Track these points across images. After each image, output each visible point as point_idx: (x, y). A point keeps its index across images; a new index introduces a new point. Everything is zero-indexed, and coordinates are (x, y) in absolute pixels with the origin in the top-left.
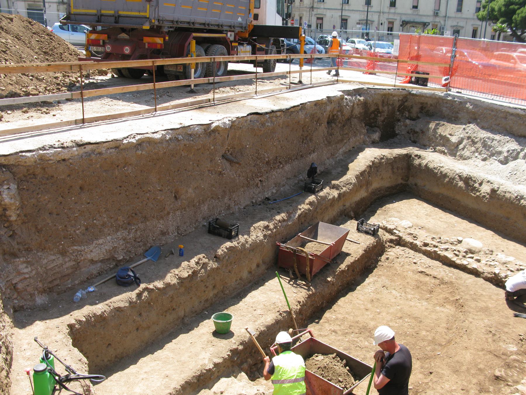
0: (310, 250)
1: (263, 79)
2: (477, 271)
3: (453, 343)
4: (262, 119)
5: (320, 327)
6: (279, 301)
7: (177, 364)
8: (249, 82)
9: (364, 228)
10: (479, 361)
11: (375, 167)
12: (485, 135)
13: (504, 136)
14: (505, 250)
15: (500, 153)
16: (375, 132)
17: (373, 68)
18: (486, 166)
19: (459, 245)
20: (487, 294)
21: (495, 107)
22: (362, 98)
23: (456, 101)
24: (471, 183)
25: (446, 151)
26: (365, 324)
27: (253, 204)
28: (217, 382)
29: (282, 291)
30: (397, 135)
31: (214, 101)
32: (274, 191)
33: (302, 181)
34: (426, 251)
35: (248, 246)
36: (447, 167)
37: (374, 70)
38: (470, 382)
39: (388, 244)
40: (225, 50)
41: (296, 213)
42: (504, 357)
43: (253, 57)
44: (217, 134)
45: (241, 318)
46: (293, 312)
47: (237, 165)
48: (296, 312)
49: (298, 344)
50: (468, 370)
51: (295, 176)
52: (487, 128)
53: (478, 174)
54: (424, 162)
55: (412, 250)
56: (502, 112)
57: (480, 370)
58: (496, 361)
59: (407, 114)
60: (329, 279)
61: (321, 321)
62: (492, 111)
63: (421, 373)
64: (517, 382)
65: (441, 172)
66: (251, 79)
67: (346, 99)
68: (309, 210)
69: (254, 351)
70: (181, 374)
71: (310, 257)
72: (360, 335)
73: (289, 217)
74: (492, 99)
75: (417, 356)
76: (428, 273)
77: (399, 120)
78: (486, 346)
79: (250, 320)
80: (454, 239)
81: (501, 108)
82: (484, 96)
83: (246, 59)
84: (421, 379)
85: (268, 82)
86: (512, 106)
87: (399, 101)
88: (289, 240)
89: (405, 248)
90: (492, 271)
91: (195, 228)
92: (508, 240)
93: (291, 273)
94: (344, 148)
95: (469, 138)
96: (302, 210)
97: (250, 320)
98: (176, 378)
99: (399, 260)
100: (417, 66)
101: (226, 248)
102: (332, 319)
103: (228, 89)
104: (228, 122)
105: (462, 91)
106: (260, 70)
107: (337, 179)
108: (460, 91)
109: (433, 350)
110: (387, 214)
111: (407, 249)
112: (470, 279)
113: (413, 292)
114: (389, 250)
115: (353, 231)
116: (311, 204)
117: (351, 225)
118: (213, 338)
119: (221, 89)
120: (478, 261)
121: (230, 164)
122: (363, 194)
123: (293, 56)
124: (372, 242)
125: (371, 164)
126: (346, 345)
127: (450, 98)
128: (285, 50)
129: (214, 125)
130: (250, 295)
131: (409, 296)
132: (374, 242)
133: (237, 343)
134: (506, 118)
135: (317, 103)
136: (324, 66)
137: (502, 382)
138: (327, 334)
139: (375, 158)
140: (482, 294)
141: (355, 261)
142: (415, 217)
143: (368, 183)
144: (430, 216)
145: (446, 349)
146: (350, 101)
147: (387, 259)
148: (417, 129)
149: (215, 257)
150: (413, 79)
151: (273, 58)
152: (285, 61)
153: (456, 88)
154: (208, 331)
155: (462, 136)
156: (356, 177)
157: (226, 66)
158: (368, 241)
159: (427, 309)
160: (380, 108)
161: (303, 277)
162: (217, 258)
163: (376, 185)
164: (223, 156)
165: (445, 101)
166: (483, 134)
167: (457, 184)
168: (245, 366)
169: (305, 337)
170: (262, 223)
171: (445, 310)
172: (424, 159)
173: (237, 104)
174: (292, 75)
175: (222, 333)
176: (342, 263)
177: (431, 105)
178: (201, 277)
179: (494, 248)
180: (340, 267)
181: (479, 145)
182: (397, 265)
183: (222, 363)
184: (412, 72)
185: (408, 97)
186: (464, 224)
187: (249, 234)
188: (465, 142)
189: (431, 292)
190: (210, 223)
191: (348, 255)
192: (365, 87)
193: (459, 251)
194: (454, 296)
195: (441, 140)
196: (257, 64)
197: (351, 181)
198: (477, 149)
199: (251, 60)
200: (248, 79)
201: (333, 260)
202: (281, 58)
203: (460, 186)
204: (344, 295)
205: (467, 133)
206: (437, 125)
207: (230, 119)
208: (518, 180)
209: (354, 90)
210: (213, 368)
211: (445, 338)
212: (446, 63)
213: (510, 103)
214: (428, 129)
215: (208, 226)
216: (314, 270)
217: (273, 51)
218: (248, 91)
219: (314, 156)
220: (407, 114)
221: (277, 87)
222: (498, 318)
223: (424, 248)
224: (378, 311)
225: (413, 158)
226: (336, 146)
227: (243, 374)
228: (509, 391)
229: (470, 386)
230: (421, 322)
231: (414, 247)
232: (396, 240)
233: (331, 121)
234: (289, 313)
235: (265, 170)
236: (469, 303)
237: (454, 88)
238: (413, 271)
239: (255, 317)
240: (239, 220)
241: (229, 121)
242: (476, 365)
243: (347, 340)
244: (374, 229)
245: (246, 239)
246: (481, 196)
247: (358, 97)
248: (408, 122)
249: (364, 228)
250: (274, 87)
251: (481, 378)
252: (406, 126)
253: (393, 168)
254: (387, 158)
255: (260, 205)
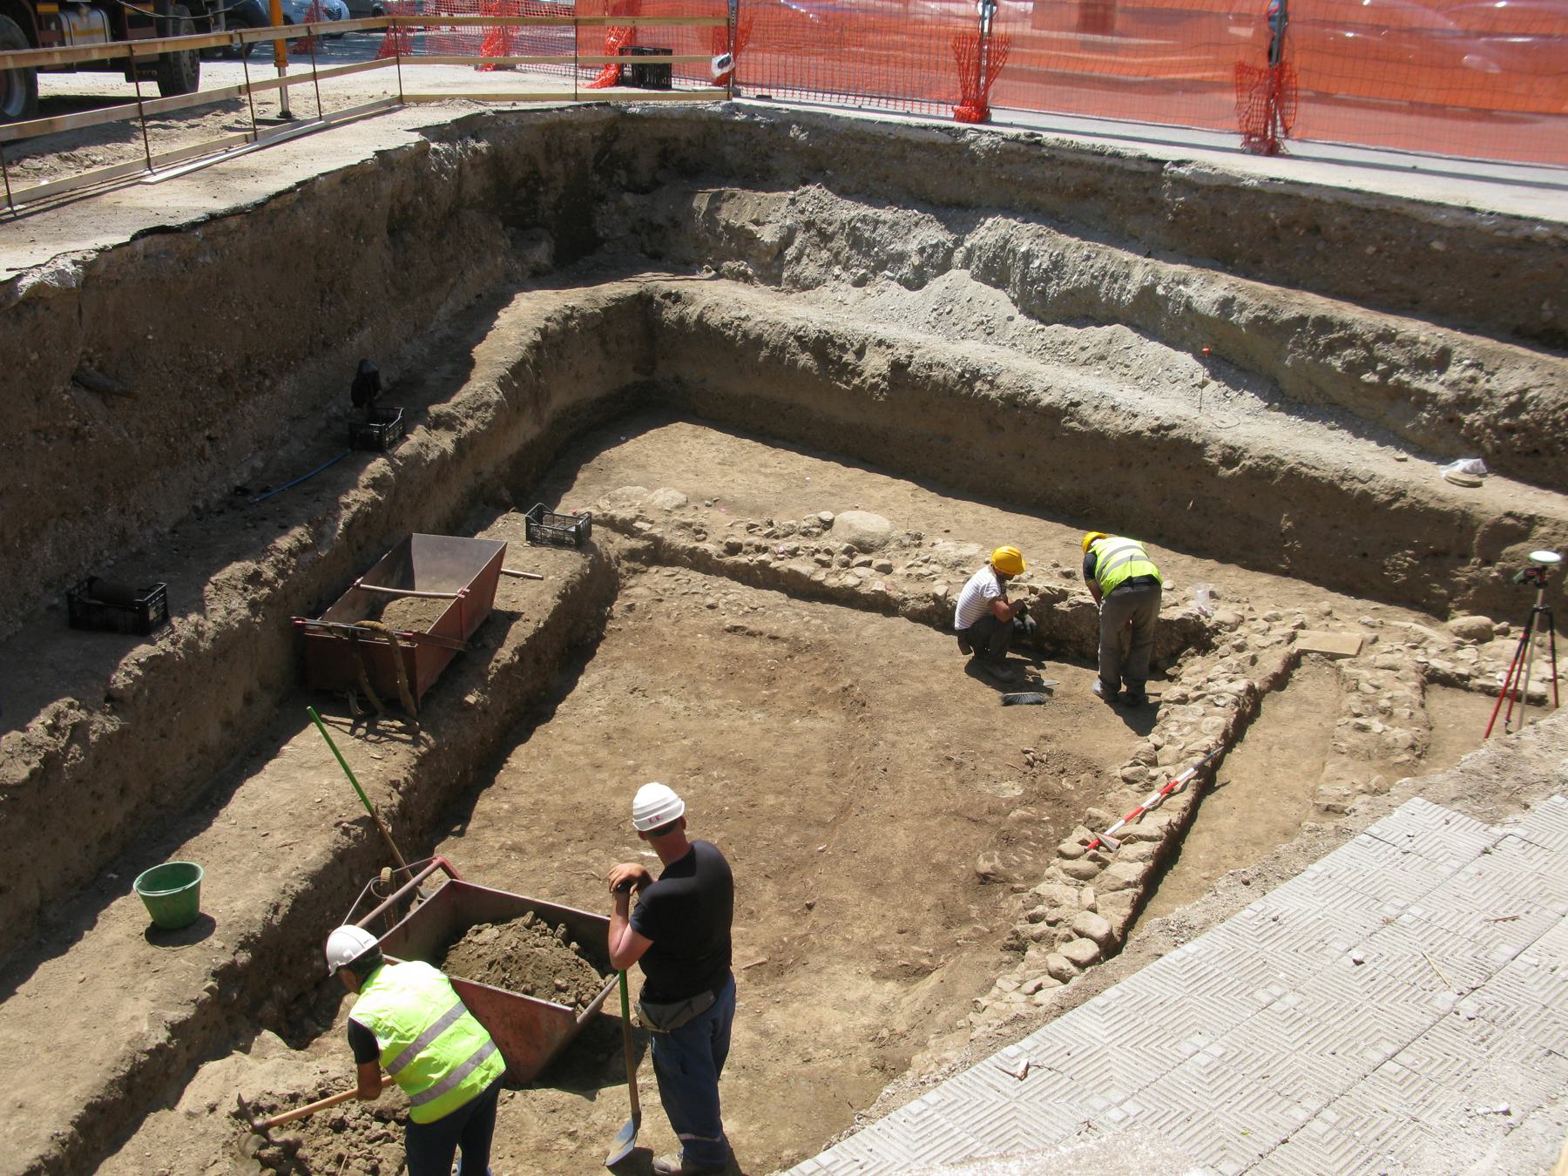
0: (399, 622)
1: (163, 116)
2: (888, 597)
3: (855, 810)
4: (184, 246)
5: (471, 844)
6: (333, 793)
7: (46, 1057)
8: (120, 132)
9: (548, 529)
10: (932, 844)
11: (552, 345)
12: (853, 213)
13: (905, 208)
14: (954, 527)
15: (901, 258)
16: (535, 241)
17: (505, 50)
18: (869, 299)
19: (826, 534)
20: (924, 656)
21: (869, 128)
22: (483, 145)
23: (759, 123)
24: (834, 353)
25: (750, 271)
26: (599, 810)
27: (200, 514)
28: (190, 1079)
29: (337, 763)
30: (603, 241)
31: (10, 205)
32: (259, 464)
33: (338, 419)
34: (737, 566)
35: (205, 645)
36: (760, 318)
37: (507, 54)
38: (917, 907)
39: (626, 564)
40: (17, 32)
41: (336, 520)
42: (994, 819)
43: (119, 49)
44: (41, 311)
45: (227, 868)
46: (381, 818)
47: (128, 402)
48: (390, 817)
49: (415, 908)
50: (907, 875)
51: (314, 408)
52: (857, 192)
53: (850, 325)
54: (693, 312)
55: (697, 570)
56: (891, 142)
57: (939, 868)
58: (977, 835)
59: (622, 176)
60: (471, 699)
61: (471, 826)
62: (863, 141)
63: (781, 913)
64: (1035, 878)
65: (745, 335)
66: (126, 121)
67: (436, 152)
68: (374, 502)
69: (286, 959)
70: (66, 1087)
71: (403, 644)
72: (591, 844)
73: (318, 536)
74: (860, 109)
75: (763, 869)
76: (752, 627)
77: (602, 199)
78: (943, 801)
79: (255, 870)
80: (808, 519)
81: (885, 131)
82: (835, 100)
83: (96, 56)
84: (785, 929)
85: (182, 125)
86: (913, 121)
87: (593, 140)
88: (331, 603)
89: (676, 569)
90: (926, 590)
91: (24, 621)
92: (956, 498)
93: (352, 701)
94: (451, 302)
95: (809, 225)
96: (355, 508)
97: (255, 870)
98: (54, 1105)
99: (663, 607)
100: (634, 32)
101: (140, 665)
102: (502, 814)
103: (52, 160)
104: (71, 269)
105: (773, 93)
106: (150, 89)
107: (444, 397)
108: (766, 92)
109: (806, 842)
110: (607, 479)
111: (683, 571)
112: (871, 625)
113: (719, 692)
114: (632, 582)
115: (517, 543)
116: (376, 484)
117: (509, 529)
118: (151, 949)
119: (27, 162)
120: (886, 570)
121: (104, 400)
122: (527, 430)
123: (250, 35)
124: (578, 566)
125: (538, 338)
126: (556, 879)
127: (740, 117)
128: (222, 17)
129: (26, 282)
130: (240, 792)
131: (712, 705)
132: (583, 567)
133: (231, 948)
134: (902, 158)
135: (348, 176)
136: (351, 58)
137: (999, 887)
138: (494, 861)
139: (548, 319)
140: (910, 662)
141: (539, 633)
142: (691, 476)
143: (538, 397)
144: (732, 464)
145: (838, 831)
146: (449, 156)
147: (631, 608)
148: (659, 219)
149: (109, 698)
150: (628, 72)
151: (188, 47)
152: (227, 54)
153: (755, 85)
154: (131, 931)
155: (788, 222)
156: (500, 385)
157: (32, 85)
158: (562, 567)
159: (768, 731)
160: (542, 166)
161: (394, 708)
162: (115, 701)
163: (561, 398)
164: (74, 378)
165: (727, 128)
166: (848, 211)
167: (796, 361)
168: (269, 1009)
169: (433, 883)
170: (236, 569)
171: (818, 725)
172: (691, 301)
173: (92, 206)
174: (257, 96)
175: (177, 925)
176: (501, 645)
177: (689, 142)
178: (73, 769)
179: (921, 526)
180: (497, 657)
181: (840, 242)
182: (661, 624)
183: (195, 1018)
184: (622, 52)
185: (620, 125)
186: (834, 474)
187: (201, 610)
188: (800, 238)
189: (770, 681)
190: (70, 596)
191: (513, 616)
192: (489, 108)
193: (828, 552)
194: (835, 681)
195: (730, 240)
196: (136, 72)
197: (486, 398)
198: (837, 254)
199: (113, 60)
200: (116, 123)
201: (472, 640)
202: (213, 43)
203: (804, 367)
204: (523, 738)
205: (802, 212)
206: (716, 198)
207: (78, 257)
208: (959, 327)
209: (456, 122)
210: (169, 1040)
211: (830, 804)
212: (715, 15)
213: (908, 114)
214: (691, 213)
215: (66, 607)
216: (420, 679)
217: (183, 24)
218: (122, 163)
219: (363, 339)
220: (622, 176)
221: (215, 139)
222: (963, 718)
223: (730, 560)
224: (631, 762)
225: (658, 304)
226: (428, 300)
227: (267, 1034)
228: (1020, 904)
229: (919, 918)
230: (756, 770)
231: (700, 562)
232: (647, 549)
233: (400, 224)
234: (371, 823)
235: (217, 405)
236: (880, 692)
237: (747, 85)
238: (710, 631)
239: (268, 856)
240: (163, 571)
241: (75, 263)
242: (926, 858)
243: (556, 864)
244: (578, 527)
245: (196, 625)
246: (866, 386)
247: (472, 143)
248: (628, 199)
249: (548, 529)
250: (206, 141)
251: (945, 888)
252: (625, 212)
253: (603, 343)
254: (583, 316)
255: (221, 512)
